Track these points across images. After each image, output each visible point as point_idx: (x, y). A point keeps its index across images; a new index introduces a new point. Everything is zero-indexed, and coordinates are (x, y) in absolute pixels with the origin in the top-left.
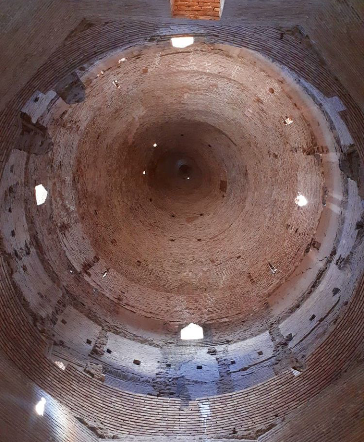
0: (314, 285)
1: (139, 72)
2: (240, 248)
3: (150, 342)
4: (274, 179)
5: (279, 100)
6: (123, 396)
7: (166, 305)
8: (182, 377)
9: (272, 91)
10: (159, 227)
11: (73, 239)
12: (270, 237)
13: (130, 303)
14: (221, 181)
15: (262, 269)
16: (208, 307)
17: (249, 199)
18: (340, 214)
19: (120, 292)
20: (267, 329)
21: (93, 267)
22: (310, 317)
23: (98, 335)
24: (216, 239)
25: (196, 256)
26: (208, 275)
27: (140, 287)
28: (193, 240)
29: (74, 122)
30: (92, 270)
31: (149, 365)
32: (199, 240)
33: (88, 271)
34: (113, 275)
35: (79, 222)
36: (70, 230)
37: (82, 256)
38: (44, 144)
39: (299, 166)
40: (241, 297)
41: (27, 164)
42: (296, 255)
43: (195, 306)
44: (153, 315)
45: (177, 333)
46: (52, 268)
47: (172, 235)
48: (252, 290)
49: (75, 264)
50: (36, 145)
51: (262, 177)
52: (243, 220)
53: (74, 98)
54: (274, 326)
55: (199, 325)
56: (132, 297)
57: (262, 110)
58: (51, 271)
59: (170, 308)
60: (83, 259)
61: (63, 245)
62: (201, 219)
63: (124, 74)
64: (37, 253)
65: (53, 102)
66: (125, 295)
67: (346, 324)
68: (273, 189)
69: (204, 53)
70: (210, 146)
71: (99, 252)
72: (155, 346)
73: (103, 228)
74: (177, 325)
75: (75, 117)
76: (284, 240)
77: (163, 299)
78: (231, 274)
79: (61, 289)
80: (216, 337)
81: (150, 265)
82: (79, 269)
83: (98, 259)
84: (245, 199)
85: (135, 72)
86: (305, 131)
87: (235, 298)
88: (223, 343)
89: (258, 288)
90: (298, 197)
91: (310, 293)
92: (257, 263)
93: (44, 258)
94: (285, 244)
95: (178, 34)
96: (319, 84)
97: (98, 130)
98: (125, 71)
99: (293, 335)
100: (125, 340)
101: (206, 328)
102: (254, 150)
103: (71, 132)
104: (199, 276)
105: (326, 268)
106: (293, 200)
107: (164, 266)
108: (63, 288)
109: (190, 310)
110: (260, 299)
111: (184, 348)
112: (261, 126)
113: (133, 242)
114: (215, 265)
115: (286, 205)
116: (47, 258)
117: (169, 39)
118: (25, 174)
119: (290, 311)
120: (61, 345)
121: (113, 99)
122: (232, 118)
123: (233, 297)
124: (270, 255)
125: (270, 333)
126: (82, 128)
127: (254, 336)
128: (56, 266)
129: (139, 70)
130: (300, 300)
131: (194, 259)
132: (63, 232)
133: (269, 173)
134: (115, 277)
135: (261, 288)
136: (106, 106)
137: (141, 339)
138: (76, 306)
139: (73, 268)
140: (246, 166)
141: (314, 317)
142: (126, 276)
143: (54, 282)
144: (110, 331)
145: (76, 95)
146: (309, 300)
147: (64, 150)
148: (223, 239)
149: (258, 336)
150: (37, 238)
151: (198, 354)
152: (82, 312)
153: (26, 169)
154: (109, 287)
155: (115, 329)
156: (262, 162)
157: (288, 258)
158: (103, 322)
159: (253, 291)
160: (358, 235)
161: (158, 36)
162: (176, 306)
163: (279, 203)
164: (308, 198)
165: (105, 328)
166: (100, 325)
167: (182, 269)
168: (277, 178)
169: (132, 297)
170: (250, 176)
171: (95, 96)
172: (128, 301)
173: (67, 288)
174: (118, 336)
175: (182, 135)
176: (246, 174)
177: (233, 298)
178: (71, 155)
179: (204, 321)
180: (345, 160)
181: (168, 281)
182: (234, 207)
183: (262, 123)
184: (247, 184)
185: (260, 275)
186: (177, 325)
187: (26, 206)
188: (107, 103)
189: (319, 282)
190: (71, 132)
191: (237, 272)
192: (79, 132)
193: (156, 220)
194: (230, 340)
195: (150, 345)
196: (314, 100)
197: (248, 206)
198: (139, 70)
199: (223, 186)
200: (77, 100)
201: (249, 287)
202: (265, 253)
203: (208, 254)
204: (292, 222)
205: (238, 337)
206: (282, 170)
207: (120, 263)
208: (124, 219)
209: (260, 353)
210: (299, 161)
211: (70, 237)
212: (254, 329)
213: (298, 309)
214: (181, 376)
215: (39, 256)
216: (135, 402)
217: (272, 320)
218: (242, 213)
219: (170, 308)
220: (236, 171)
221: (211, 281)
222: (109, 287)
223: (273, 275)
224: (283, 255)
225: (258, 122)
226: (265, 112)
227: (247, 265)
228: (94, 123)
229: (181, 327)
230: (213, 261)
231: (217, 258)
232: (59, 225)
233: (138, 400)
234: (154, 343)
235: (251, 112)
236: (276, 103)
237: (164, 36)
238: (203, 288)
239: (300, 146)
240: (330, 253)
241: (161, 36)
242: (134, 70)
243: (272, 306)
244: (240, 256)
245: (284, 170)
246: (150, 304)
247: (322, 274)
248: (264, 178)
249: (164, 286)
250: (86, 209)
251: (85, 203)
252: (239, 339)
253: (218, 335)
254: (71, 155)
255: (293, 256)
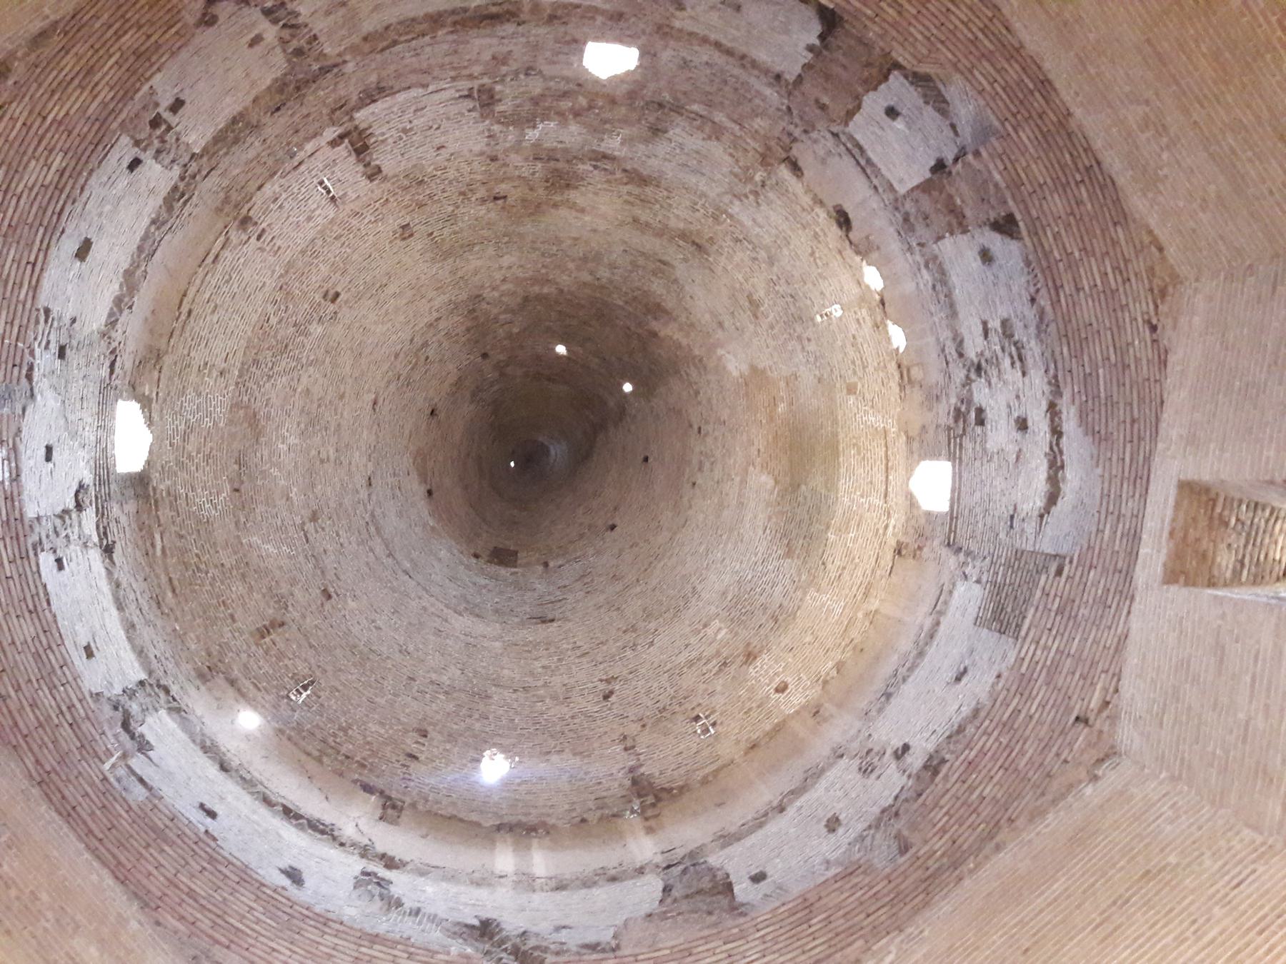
0: (289, 813)
1: (850, 372)
2: (349, 601)
3: (126, 299)
4: (542, 692)
5: (759, 707)
6: (57, 193)
7: (206, 364)
8: (32, 395)
9: (781, 689)
10: (412, 369)
11: (448, 119)
12: (386, 683)
13: (226, 253)
14: (516, 553)
15: (298, 662)
16: (190, 494)
17: (480, 628)
18: (497, 872)
19: (264, 225)
20: (150, 673)
21: (353, 158)
22: (208, 805)
23: (183, 139)
24: (372, 529)
25: (329, 467)
26: (278, 502)
27: (266, 289)
28: (370, 464)
29: (759, 189)
30: (345, 154)
31: (70, 287)
32: (49, 449)
33: (346, 141)
34: (317, 213)
35: (488, 145)
36: (474, 114)
37: (393, 132)
38: (818, 111)
39: (589, 756)
40: (218, 597)
41: (718, 45)
42: (347, 757)
43: (194, 454)
44: (183, 317)
45: (134, 392)
46: (408, 41)
47: (387, 402)
48: (239, 630)
49: (377, 107)
50: (825, 89)
51: (545, 662)
52: (425, 609)
53: (918, 210)
54: (162, 695)
55: (148, 462)
56: (242, 260)
57: (725, 664)
58: (400, 35)
59: (194, 375)
60: (383, 134)
61: (443, 85)
62: (421, 490)
63: (854, 337)
64: (465, 10)
65: (856, 151)
66: (253, 239)
67: (280, 913)
68: (515, 691)
69: (881, 531)
70: (613, 527)
71: (387, 185)
72: (111, 314)
73: (451, 209)
74: (151, 392)
75: (771, 195)
76: (382, 724)
77: (224, 355)
78: (280, 568)
79: (339, 55)
80: (119, 512)
81: (320, 330)
82: (361, 116)
83: (371, 178)
84: (478, 616)
85: (853, 362)
86: (682, 771)
87: (214, 578)
88: (103, 534)
89: (245, 647)
90: (500, 757)
91: (267, 801)
92: (311, 646)
93: (443, 26)
94: (373, 727)
95: (960, 477)
96: (936, 805)
97: (715, 247)
98: (860, 340)
99: (150, 753)
100: (146, 221)
101: (140, 483)
102: (616, 641)
103: (736, 176)
104: (275, 472)
105: (342, 845)
106: (495, 745)
107: (311, 369)
108: (339, 60)
109: (185, 438)
110: (215, 653)
111: (95, 410)
112: (682, 659)
113: (392, 289)
114: (303, 523)
115: (477, 726)
116: (440, 33)
117: (951, 457)
118: (691, 34)
119: (208, 743)
120: (204, 15)
121: (789, 299)
122: (699, 588)
123: (216, 572)
124: (337, 684)
125: (141, 683)
126: (736, 208)
127: (127, 632)
128: (404, 57)
129: (855, 373)
130: (243, 773)
131: (322, 461)
132: (476, 95)
133: (557, 681)
134: (309, 219)
135: (244, 656)
136: (775, 278)
137: (139, 273)
138: (280, 86)
139: (362, 104)
140: (567, 620)
141: (212, 814)
142: (303, 252)
143: (365, 39)
144: (182, 178)
145: (926, 218)
146: (248, 798)
147: (694, 147)
148: (371, 550)
149: (128, 647)
150: (508, 20)
151: (81, 453)
152: (255, 100)
153: (705, 40)
154: (284, 196)
155: (183, 195)
156: (584, 660)
157: (335, 735)
158: (213, 162)
159: (237, 634)
160: (466, 926)
161: (964, 430)
162: (199, 395)
163: (481, 707)
164: (506, 784)
165: (194, 164)
166: (205, 150)
167: (299, 424)
168: (547, 701)
169: (242, 260)
170: (542, 632)
171: (812, 254)
172: (235, 248)
173: (336, 70)
174: (160, 201)
175: (646, 459)
176: (544, 620)
177: (212, 571)
178: (673, 164)
179: (155, 476)
180: (715, 876)
181: (270, 377)
182: (452, 585)
183: (691, 664)
184: (516, 620)
185: (281, 656)
186: (151, 392)
187: (603, 12)
188: (782, 281)
189: (300, 827)
190: (736, 176)
191: (284, 589)
192: (727, 199)
193: (431, 363)
194: (114, 556)
195: (118, 301)
196: (792, 792)
197: (461, 623)
198: (855, 373)
199: (502, 557)
200: (912, 219)
201: (248, 622)
202: (340, 670)
203: (332, 505)
204: (435, 743)
205: (124, 579)
206: (571, 714)
207: (343, 239)
208: (460, 274)
209: (89, 652)
210: (601, 756)
211: (453, 110)
212: (146, 634)
213: (217, 767)
214: (36, 391)
215: (454, 12)
216: (34, 230)
217: (174, 689)
218: (442, 606)
219: (194, 375)
220: (549, 594)
221: (260, 509)
222: (284, 196)
223: (284, 693)
224: (343, 719)
225: (694, 653)
226: (720, 670)
227: (304, 617)
228: (737, 240)
229: (145, 403)
230: (314, 518)
231: (323, 529)
232: (498, 88)
233: (38, 242)
234: (121, 311)
235: (719, 637)
236: (749, 699)
237: (961, 445)
238: (242, 482)
239: (642, 757)
240: (390, 853)
241: (961, 437)
242: (858, 362)
243: (209, 690)
244: (329, 597)
245: (573, 717)
246: (213, 312)
247: (323, 832)
248: (543, 667)
249: (256, 362)
250: (517, 173)
251: (533, 174)
252: (118, 585)
253: (123, 519)
254: (673, 164)
255: (343, 750)
